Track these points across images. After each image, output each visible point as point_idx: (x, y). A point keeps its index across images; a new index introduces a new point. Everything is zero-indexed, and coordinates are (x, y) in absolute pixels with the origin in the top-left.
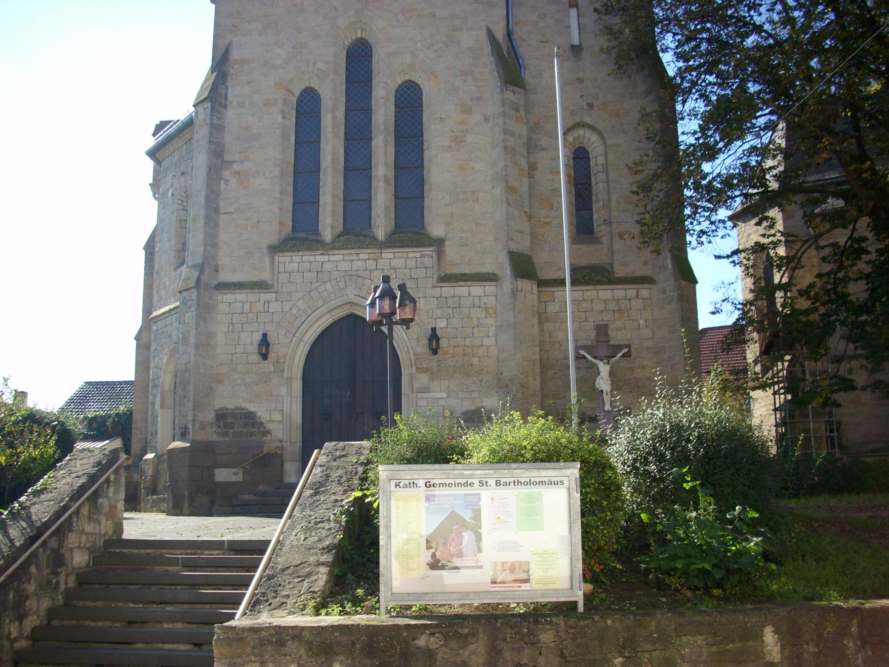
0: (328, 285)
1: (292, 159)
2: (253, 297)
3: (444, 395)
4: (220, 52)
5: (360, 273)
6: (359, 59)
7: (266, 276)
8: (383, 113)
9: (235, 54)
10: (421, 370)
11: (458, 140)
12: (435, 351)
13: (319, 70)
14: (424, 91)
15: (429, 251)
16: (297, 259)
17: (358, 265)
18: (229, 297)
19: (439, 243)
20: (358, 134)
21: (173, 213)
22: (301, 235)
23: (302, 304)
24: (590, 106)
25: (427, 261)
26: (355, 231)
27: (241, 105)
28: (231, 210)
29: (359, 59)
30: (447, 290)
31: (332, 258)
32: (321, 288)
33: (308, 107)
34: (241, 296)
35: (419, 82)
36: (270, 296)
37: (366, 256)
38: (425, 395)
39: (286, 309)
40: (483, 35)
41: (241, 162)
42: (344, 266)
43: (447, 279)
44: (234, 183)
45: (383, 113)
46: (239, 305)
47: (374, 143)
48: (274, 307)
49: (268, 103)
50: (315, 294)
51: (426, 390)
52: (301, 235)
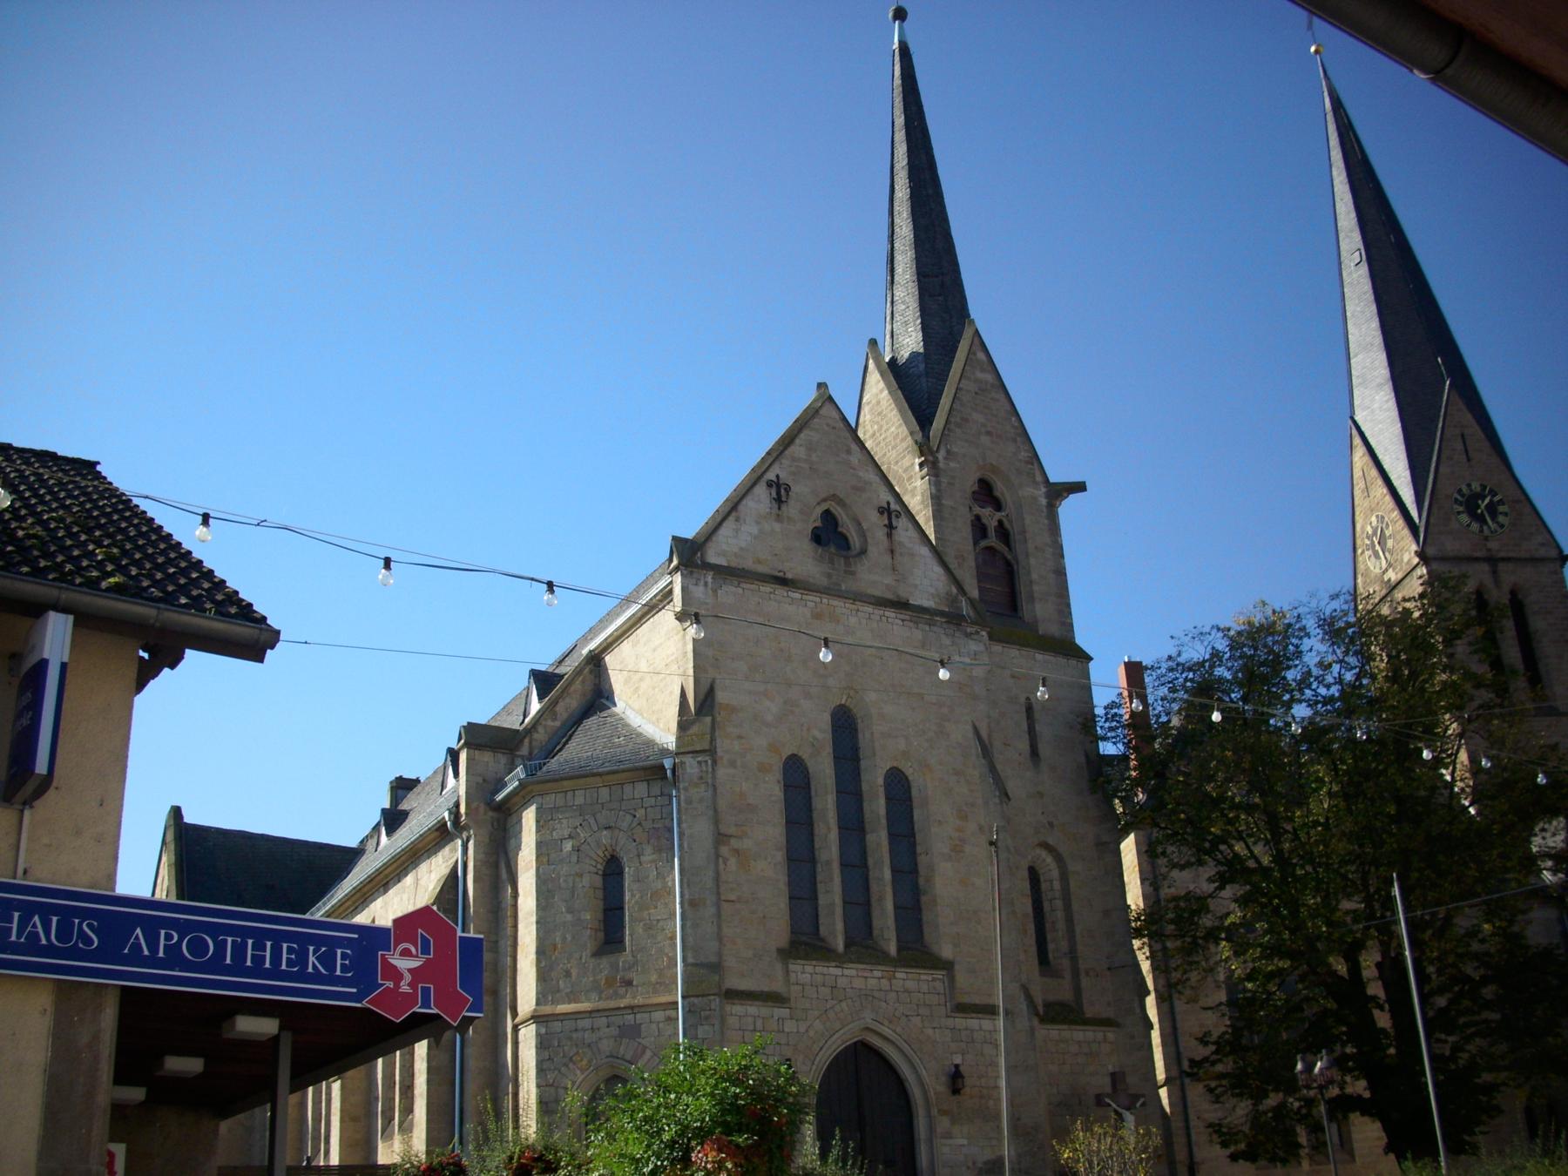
0: (844, 1004)
1: (865, 804)
2: (765, 1011)
3: (965, 1142)
4: (702, 697)
5: (876, 994)
6: (845, 726)
7: (778, 986)
8: (877, 807)
9: (721, 696)
10: (943, 1112)
11: (957, 850)
12: (956, 1091)
13: (815, 738)
14: (914, 785)
15: (939, 974)
16: (809, 969)
17: (872, 982)
18: (738, 1008)
19: (948, 966)
20: (853, 825)
21: (1334, 597)
22: (805, 942)
23: (818, 1025)
24: (1051, 824)
25: (938, 985)
26: (862, 946)
27: (733, 764)
28: (733, 897)
29: (845, 726)
30: (960, 1022)
31: (846, 972)
32: (837, 1008)
33: (796, 775)
34: (752, 1009)
35: (909, 772)
36: (785, 1012)
37: (879, 974)
38: (949, 1141)
39: (802, 1030)
40: (969, 728)
41: (740, 837)
42: (858, 983)
43: (962, 1009)
44: (733, 862)
45: (877, 807)
46: (750, 1020)
47: (870, 838)
48: (790, 1026)
49: (763, 768)
50: (831, 1014)
51: (948, 1135)
52: (805, 942)
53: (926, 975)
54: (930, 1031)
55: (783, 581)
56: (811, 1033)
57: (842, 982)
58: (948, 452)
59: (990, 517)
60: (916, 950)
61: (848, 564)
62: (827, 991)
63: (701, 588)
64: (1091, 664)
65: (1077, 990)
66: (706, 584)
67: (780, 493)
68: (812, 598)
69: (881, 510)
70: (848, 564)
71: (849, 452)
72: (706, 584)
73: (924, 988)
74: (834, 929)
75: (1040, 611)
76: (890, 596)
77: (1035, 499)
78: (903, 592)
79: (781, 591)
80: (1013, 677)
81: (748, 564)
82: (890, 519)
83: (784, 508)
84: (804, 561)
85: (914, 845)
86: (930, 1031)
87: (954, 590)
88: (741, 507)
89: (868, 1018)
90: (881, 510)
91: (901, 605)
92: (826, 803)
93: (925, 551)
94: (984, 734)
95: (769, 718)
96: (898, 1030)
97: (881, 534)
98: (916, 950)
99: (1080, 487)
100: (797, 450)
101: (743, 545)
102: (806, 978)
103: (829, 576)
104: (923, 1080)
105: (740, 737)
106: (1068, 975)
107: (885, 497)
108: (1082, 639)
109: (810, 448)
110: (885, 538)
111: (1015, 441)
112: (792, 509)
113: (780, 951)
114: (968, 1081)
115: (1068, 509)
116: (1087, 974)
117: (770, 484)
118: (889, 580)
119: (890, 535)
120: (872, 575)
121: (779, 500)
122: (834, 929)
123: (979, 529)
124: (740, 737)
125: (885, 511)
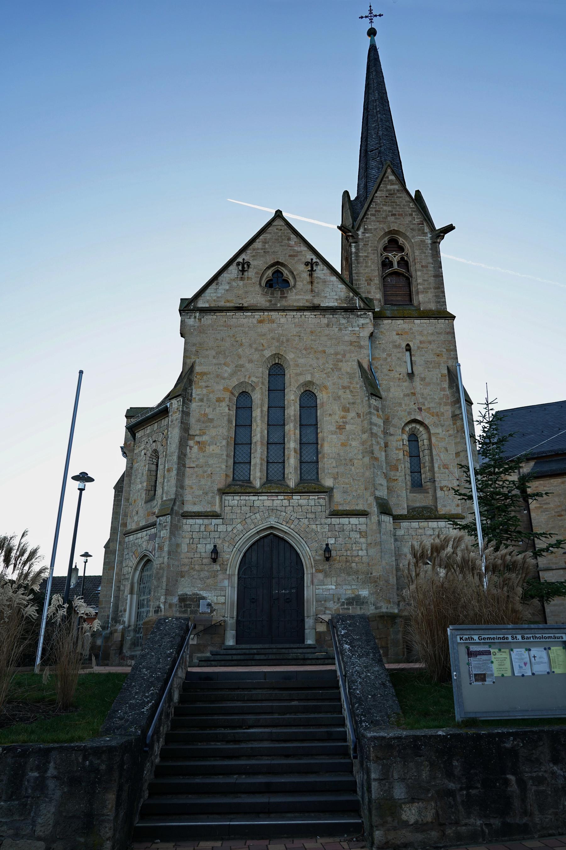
0: (257, 515)
5: (279, 508)
6: (277, 371)
8: (292, 410)
19: (329, 491)
20: (276, 423)
23: (240, 527)
24: (420, 409)
26: (275, 484)
29: (277, 371)
30: (335, 521)
32: (253, 517)
33: (243, 403)
36: (219, 521)
41: (200, 435)
42: (268, 503)
43: (335, 514)
45: (292, 410)
48: (221, 528)
50: (248, 521)
53: (313, 497)
54: (314, 527)
55: (240, 309)
56: (235, 531)
57: (257, 503)
58: (365, 229)
59: (395, 258)
60: (310, 484)
61: (282, 293)
62: (248, 508)
63: (192, 320)
64: (456, 322)
65: (435, 498)
66: (195, 317)
67: (244, 267)
68: (257, 315)
69: (307, 264)
70: (282, 293)
71: (289, 239)
72: (195, 317)
73: (312, 503)
74: (257, 477)
75: (424, 300)
76: (308, 304)
77: (423, 241)
78: (316, 301)
79: (239, 314)
80: (398, 334)
81: (222, 304)
82: (312, 267)
83: (246, 273)
84: (257, 297)
85: (317, 428)
86: (314, 527)
87: (351, 294)
88: (220, 279)
89: (272, 521)
90: (307, 264)
91: (315, 308)
92: (259, 415)
93: (334, 279)
94: (365, 366)
95: (226, 375)
96: (292, 526)
97: (306, 276)
98: (310, 484)
99: (450, 228)
100: (258, 244)
101: (219, 295)
102: (231, 503)
103: (270, 301)
104: (308, 553)
105: (207, 387)
106: (431, 491)
107: (310, 256)
108: (450, 309)
109: (265, 242)
110: (308, 278)
111: (411, 215)
112: (251, 273)
113: (219, 490)
114: (333, 553)
115: (445, 245)
116: (442, 489)
117: (238, 264)
118: (309, 297)
119: (311, 275)
120: (298, 296)
121: (243, 271)
122: (257, 477)
123: (386, 264)
124: (207, 387)
125: (311, 264)
